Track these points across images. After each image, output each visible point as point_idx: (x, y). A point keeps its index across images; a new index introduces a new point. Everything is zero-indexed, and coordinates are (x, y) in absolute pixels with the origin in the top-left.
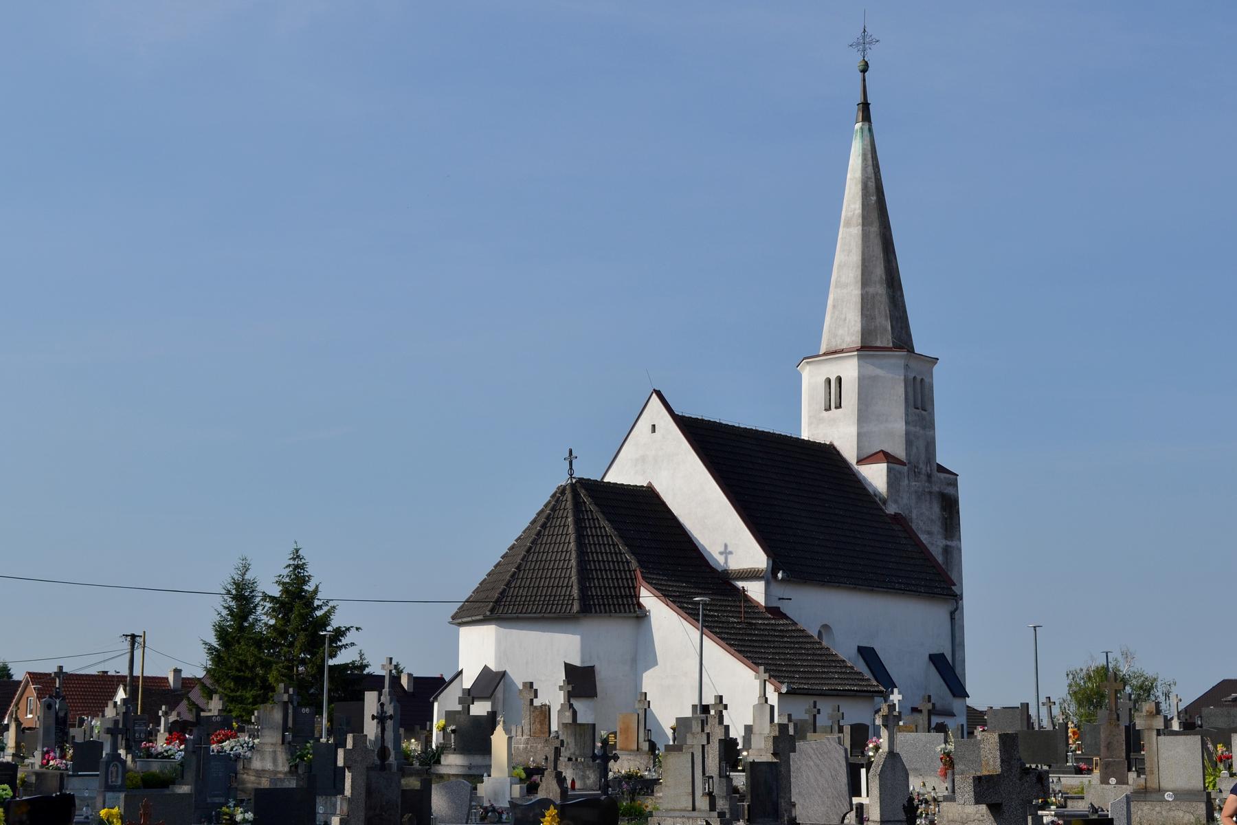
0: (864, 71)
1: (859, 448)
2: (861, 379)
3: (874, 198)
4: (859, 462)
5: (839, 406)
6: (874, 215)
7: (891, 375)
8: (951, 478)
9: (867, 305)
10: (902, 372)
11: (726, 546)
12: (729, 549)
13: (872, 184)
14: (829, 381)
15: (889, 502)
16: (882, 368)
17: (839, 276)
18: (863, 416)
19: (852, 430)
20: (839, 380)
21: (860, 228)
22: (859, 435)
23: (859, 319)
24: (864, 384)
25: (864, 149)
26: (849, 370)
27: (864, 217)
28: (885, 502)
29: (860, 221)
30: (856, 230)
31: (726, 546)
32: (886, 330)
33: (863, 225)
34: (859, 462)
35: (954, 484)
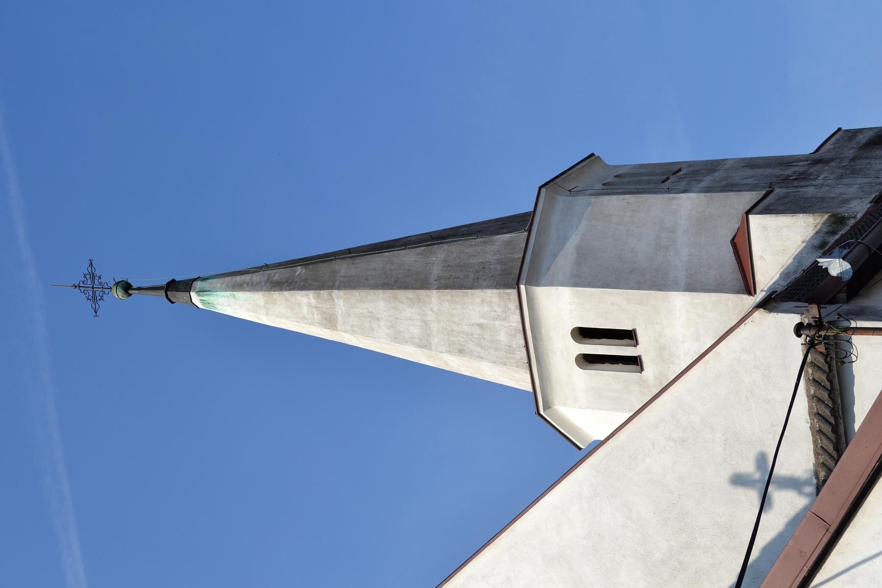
0: (127, 288)
1: (719, 288)
2: (578, 280)
3: (299, 270)
4: (749, 288)
5: (629, 336)
6: (324, 269)
7: (584, 223)
8: (844, 137)
9: (458, 280)
10: (582, 200)
11: (739, 480)
12: (748, 467)
13: (278, 275)
14: (588, 360)
15: (842, 210)
16: (564, 239)
17: (410, 341)
18: (653, 278)
19: (679, 302)
20: (584, 334)
21: (336, 293)
22: (690, 288)
23: (479, 295)
24: (591, 274)
25: (226, 289)
26: (563, 307)
27: (321, 287)
28: (837, 221)
29: (324, 293)
30: (341, 301)
31: (739, 480)
32: (509, 242)
33: (331, 287)
34: (749, 288)
35: (853, 134)
